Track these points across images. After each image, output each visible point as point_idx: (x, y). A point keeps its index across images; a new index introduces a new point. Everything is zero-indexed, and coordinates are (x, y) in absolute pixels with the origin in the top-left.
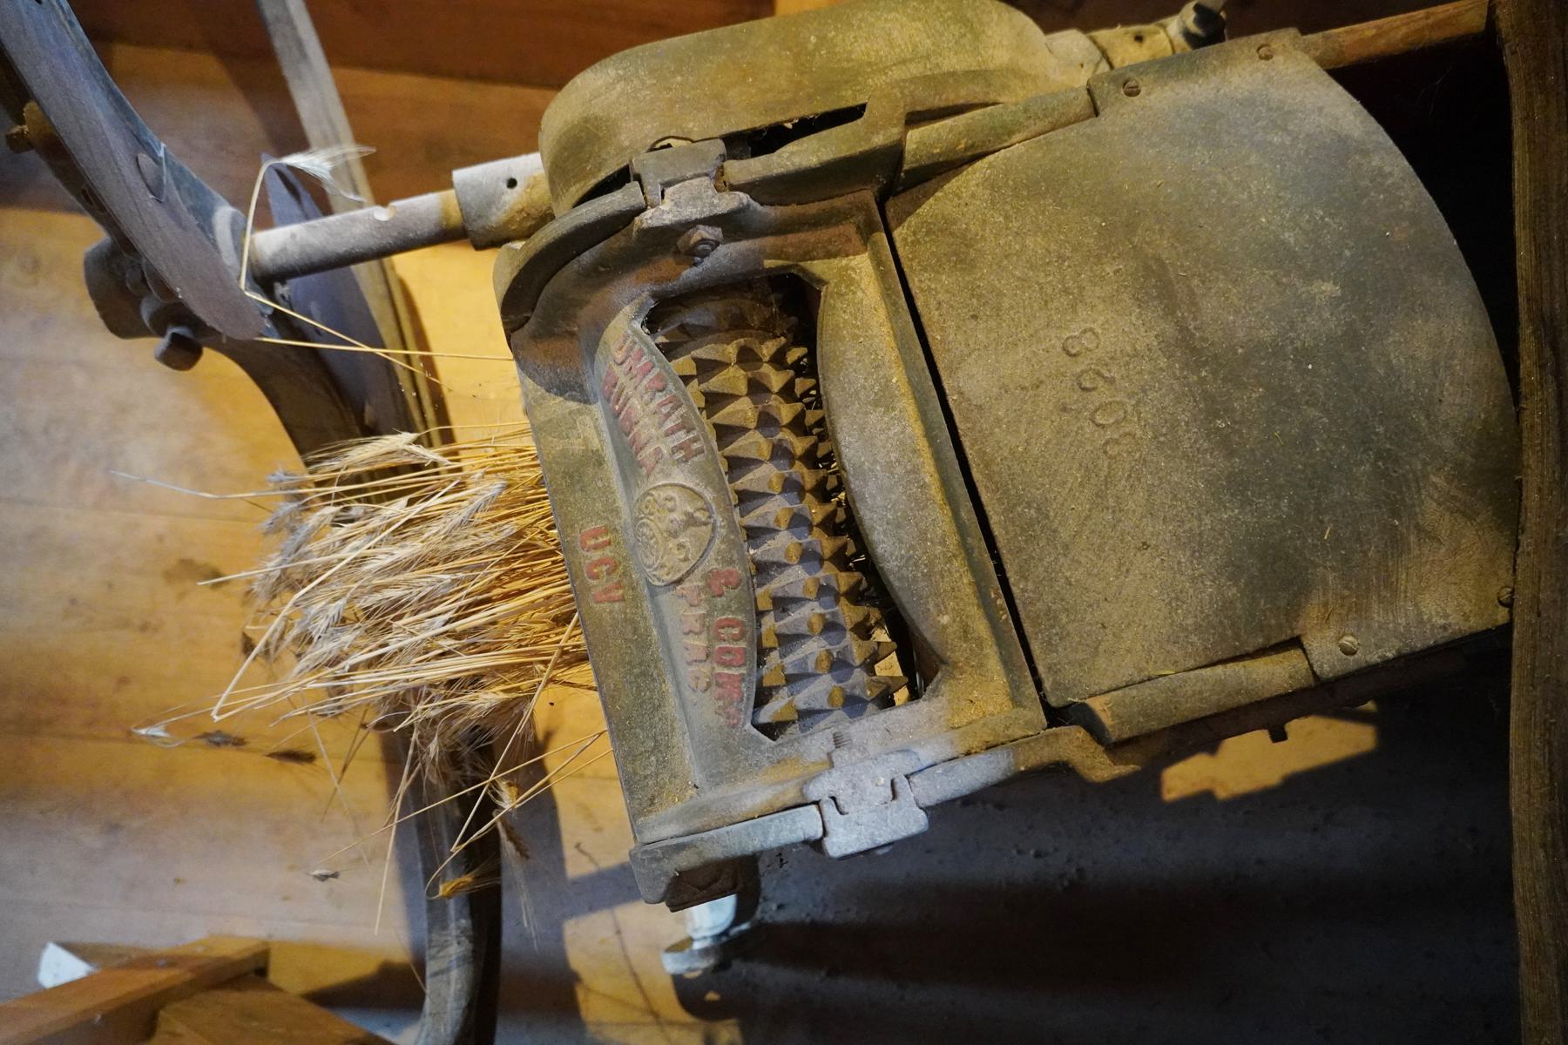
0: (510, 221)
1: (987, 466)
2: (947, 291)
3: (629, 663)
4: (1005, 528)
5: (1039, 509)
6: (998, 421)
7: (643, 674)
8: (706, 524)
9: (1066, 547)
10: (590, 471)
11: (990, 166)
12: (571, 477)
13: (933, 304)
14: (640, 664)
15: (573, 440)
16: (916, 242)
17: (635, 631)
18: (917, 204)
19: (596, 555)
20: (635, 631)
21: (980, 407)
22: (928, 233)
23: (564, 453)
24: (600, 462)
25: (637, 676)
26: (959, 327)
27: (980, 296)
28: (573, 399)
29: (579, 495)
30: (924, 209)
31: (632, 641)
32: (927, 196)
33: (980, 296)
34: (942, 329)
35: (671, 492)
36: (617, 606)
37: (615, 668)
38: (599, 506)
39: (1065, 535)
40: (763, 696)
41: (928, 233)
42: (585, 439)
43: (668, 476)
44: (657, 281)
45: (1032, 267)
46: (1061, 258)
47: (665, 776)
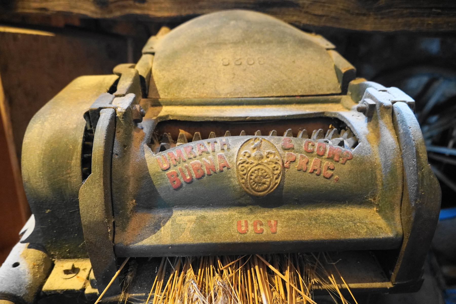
0: (34, 275)
1: (256, 92)
2: (191, 89)
3: (309, 224)
4: (278, 92)
5: (275, 83)
6: (242, 86)
7: (315, 220)
8: (261, 141)
9: (289, 78)
10: (206, 222)
11: (156, 69)
12: (206, 232)
13: (193, 94)
14: (310, 220)
15: (187, 227)
16: (168, 93)
17: (293, 219)
18: (156, 89)
19: (251, 228)
20: (293, 219)
21: (235, 90)
22: (167, 89)
23: (191, 232)
24: (204, 217)
25: (317, 223)
26: (205, 89)
27: (198, 81)
28: (165, 222)
29: (217, 230)
30: (158, 87)
31: (298, 222)
32: (155, 85)
33: (198, 81)
34: (203, 93)
35: (242, 152)
36: (279, 224)
37: (311, 230)
38: (226, 222)
39: (285, 78)
40: (308, 254)
41: (167, 89)
42: (189, 221)
43: (233, 155)
44: (142, 139)
45: (195, 67)
46: (197, 61)
47: (367, 221)
